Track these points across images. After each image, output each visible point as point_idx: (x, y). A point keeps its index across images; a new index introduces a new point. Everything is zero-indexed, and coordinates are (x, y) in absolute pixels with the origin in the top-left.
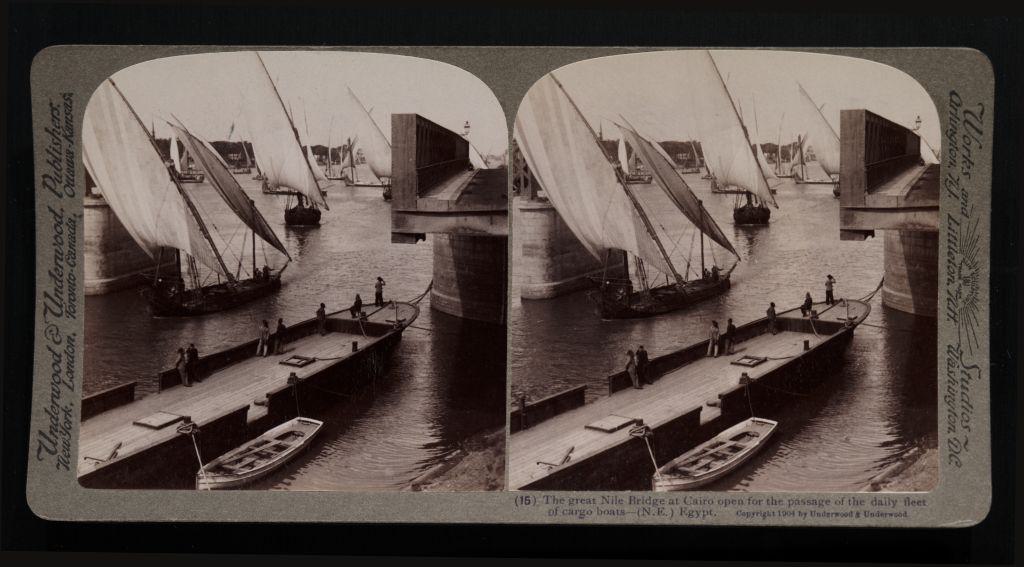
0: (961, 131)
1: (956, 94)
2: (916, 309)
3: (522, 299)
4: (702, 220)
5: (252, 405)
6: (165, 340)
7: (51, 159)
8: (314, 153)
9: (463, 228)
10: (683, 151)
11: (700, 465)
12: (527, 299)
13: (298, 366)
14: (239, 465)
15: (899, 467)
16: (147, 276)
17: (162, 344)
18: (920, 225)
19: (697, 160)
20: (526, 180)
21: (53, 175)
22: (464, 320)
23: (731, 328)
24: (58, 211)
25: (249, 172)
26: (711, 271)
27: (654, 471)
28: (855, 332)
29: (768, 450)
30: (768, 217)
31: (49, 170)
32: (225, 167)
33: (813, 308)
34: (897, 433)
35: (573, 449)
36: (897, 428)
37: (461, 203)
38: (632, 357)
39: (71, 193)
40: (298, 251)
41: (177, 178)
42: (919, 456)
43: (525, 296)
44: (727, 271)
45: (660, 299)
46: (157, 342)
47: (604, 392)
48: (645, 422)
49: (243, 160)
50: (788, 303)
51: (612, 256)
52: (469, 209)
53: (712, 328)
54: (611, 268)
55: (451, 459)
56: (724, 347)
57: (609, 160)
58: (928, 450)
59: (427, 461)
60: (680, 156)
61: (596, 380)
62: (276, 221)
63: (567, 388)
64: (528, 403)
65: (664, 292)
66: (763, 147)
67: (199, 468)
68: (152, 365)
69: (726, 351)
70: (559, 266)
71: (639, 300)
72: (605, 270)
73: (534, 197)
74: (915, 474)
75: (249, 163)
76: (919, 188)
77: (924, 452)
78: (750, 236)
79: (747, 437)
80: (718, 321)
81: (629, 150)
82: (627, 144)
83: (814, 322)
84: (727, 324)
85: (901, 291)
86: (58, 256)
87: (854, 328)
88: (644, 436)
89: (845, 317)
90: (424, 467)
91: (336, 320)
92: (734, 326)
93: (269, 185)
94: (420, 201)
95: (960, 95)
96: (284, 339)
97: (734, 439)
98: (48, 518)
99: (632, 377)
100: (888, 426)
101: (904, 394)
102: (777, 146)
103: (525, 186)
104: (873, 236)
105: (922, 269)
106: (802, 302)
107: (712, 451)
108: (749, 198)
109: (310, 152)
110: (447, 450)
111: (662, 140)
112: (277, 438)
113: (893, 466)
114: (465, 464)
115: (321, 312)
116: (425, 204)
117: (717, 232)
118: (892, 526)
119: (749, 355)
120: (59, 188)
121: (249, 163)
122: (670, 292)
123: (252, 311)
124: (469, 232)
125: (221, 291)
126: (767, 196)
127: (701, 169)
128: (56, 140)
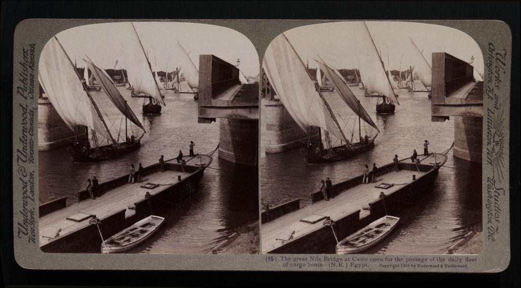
0: (495, 64)
1: (492, 45)
4: (127, 112)
5: (127, 210)
6: (314, 176)
10: (350, 74)
11: (360, 240)
12: (268, 153)
18: (473, 113)
20: (268, 90)
21: (22, 87)
23: (375, 168)
24: (25, 106)
26: (130, 138)
28: (439, 170)
31: (21, 85)
32: (344, 83)
37: (468, 99)
38: (90, 182)
39: (31, 97)
41: (87, 89)
52: (238, 105)
53: (365, 168)
56: (371, 179)
58: (477, 233)
59: (454, 238)
60: (349, 77)
62: (138, 112)
63: (290, 200)
64: (270, 208)
66: (157, 72)
72: (76, 136)
75: (125, 80)
76: (472, 94)
77: (476, 234)
78: (151, 120)
80: (368, 164)
81: (322, 74)
89: (434, 162)
90: (218, 242)
92: (142, 167)
96: (376, 174)
99: (324, 194)
105: (474, 137)
106: (412, 155)
109: (390, 74)
113: (460, 241)
114: (239, 240)
115: (161, 160)
120: (26, 94)
121: (125, 80)
122: (110, 149)
124: (238, 117)
128: (25, 69)
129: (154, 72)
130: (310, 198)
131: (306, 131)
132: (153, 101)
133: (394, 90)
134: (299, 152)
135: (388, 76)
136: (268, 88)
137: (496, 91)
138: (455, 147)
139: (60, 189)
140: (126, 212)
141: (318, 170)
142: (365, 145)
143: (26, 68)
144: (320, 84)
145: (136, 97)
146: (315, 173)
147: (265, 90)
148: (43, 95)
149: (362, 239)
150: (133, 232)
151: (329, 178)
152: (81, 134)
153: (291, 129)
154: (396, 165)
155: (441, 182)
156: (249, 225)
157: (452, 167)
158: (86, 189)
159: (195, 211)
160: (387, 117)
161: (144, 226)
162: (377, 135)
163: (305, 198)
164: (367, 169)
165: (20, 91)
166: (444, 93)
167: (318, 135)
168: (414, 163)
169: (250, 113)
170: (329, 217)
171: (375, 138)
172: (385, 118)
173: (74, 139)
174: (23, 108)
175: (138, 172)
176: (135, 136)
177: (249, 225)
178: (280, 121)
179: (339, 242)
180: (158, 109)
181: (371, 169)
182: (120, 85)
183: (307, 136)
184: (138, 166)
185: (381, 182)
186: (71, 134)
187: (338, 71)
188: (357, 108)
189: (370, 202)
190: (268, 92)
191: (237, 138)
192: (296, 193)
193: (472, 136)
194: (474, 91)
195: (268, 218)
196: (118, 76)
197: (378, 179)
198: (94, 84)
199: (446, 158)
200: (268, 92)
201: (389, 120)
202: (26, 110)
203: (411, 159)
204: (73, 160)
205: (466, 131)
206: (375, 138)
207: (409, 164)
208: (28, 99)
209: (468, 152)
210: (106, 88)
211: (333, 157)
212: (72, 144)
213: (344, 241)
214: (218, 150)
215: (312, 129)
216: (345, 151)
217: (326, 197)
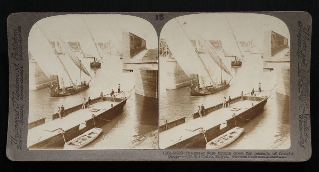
0: (302, 35)
1: (301, 23)
2: (145, 94)
4: (81, 68)
6: (194, 103)
9: (285, 66)
10: (74, 45)
11: (220, 141)
12: (168, 90)
14: (219, 142)
15: (138, 143)
16: (188, 83)
18: (146, 68)
19: (220, 46)
20: (168, 52)
21: (15, 53)
23: (90, 100)
24: (17, 65)
26: (83, 82)
31: (14, 52)
33: (114, 94)
36: (138, 131)
37: (285, 59)
38: (60, 109)
41: (199, 53)
42: (145, 140)
44: (229, 81)
45: (68, 91)
47: (191, 119)
48: (203, 128)
49: (218, 46)
50: (247, 92)
51: (54, 77)
52: (146, 62)
53: (84, 100)
55: (142, 140)
56: (228, 105)
57: (193, 46)
58: (148, 138)
59: (134, 141)
60: (215, 45)
64: (168, 122)
65: (69, 88)
66: (98, 43)
68: (190, 111)
69: (228, 107)
70: (178, 79)
71: (62, 91)
74: (143, 145)
75: (79, 48)
76: (146, 57)
77: (146, 138)
79: (93, 134)
80: (85, 98)
81: (199, 43)
82: (58, 42)
83: (255, 97)
84: (228, 98)
85: (140, 89)
86: (17, 80)
87: (126, 100)
88: (62, 133)
90: (133, 142)
91: (106, 98)
92: (231, 99)
94: (131, 59)
96: (230, 102)
99: (59, 115)
101: (141, 121)
105: (147, 82)
106: (111, 92)
109: (97, 45)
114: (146, 141)
115: (102, 95)
117: (85, 70)
118: (226, 161)
120: (17, 57)
122: (212, 88)
123: (80, 95)
124: (146, 69)
126: (241, 58)
127: (80, 50)
128: (16, 42)
129: (238, 42)
130: (51, 117)
132: (96, 60)
133: (100, 54)
136: (168, 51)
137: (303, 52)
138: (136, 88)
141: (57, 101)
145: (86, 58)
148: (172, 56)
153: (181, 75)
155: (127, 108)
162: (231, 79)
163: (188, 116)
165: (14, 56)
167: (57, 80)
170: (202, 128)
172: (96, 71)
174: (16, 65)
176: (226, 80)
179: (208, 142)
181: (87, 100)
182: (76, 51)
186: (189, 79)
187: (209, 41)
190: (168, 54)
191: (146, 81)
194: (147, 55)
195: (166, 128)
197: (91, 106)
199: (131, 94)
200: (168, 54)
202: (18, 67)
207: (109, 98)
208: (19, 60)
209: (143, 91)
212: (189, 85)
213: (210, 142)
214: (134, 88)
217: (201, 116)
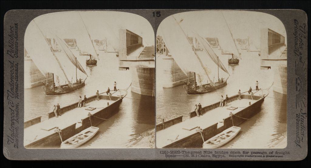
0: (299, 33)
3: (163, 88)
5: (77, 123)
6: (50, 102)
7: (10, 45)
8: (237, 41)
9: (140, 65)
10: (213, 41)
11: (75, 141)
13: (91, 110)
15: (135, 142)
17: (49, 104)
20: (165, 49)
22: (142, 95)
23: (85, 98)
25: (217, 47)
26: (79, 80)
27: (61, 143)
28: (123, 100)
29: (239, 134)
30: (96, 63)
31: (9, 49)
32: (209, 45)
33: (110, 92)
34: (277, 131)
35: (37, 136)
36: (135, 130)
37: (140, 57)
39: (17, 56)
40: (90, 74)
41: (195, 50)
43: (164, 87)
46: (47, 103)
49: (215, 44)
52: (143, 59)
53: (79, 98)
54: (190, 78)
58: (144, 137)
60: (212, 42)
61: (186, 114)
62: (84, 65)
63: (177, 116)
64: (165, 121)
66: (237, 40)
67: (203, 142)
69: (225, 105)
70: (174, 77)
71: (57, 89)
72: (47, 79)
73: (167, 55)
76: (142, 54)
77: (143, 137)
78: (233, 68)
81: (196, 40)
84: (84, 97)
89: (120, 95)
92: (86, 98)
93: (81, 53)
95: (298, 21)
97: (227, 133)
98: (12, 159)
100: (132, 129)
102: (99, 40)
103: (164, 51)
104: (129, 69)
105: (143, 80)
106: (107, 90)
107: (79, 137)
108: (233, 56)
109: (94, 42)
110: (137, 136)
111: (206, 38)
112: (85, 133)
113: (134, 142)
114: (143, 140)
115: (98, 93)
116: (272, 56)
118: (223, 160)
119: (90, 107)
120: (13, 54)
121: (217, 44)
122: (67, 87)
125: (66, 87)
130: (189, 115)
131: (45, 76)
134: (41, 88)
135: (92, 42)
136: (164, 49)
137: (300, 50)
139: (37, 112)
140: (76, 125)
142: (221, 84)
143: (13, 38)
144: (195, 46)
146: (192, 100)
147: (162, 50)
149: (76, 140)
150: (222, 136)
151: (58, 104)
152: (49, 78)
154: (98, 97)
155: (123, 107)
156: (149, 132)
157: (130, 98)
158: (53, 111)
159: (117, 123)
160: (235, 67)
161: (228, 133)
164: (81, 99)
166: (126, 53)
167: (52, 78)
168: (108, 95)
169: (149, 64)
171: (85, 80)
172: (91, 68)
173: (45, 81)
174: (11, 63)
175: (225, 100)
176: (81, 79)
177: (149, 132)
178: (172, 69)
180: (95, 62)
181: (83, 99)
182: (72, 48)
183: (187, 78)
184: (226, 97)
185: (89, 107)
186: (186, 77)
188: (75, 62)
189: (223, 118)
192: (181, 112)
193: (284, 79)
196: (71, 43)
198: (199, 46)
201: (235, 68)
203: (248, 92)
204: (45, 94)
205: (280, 76)
206: (85, 80)
208: (15, 57)
210: (206, 49)
211: (61, 91)
215: (48, 74)
216: (210, 87)
